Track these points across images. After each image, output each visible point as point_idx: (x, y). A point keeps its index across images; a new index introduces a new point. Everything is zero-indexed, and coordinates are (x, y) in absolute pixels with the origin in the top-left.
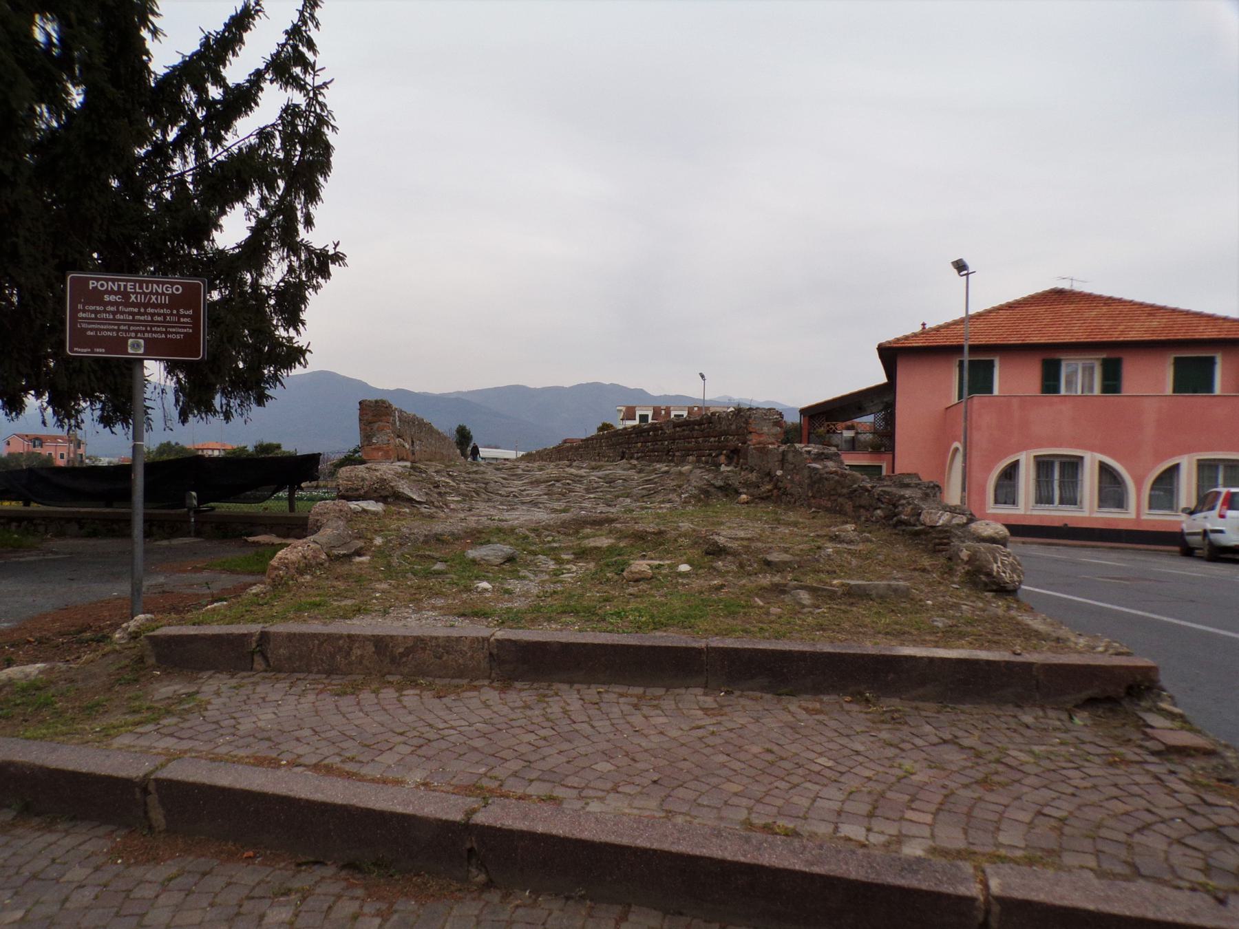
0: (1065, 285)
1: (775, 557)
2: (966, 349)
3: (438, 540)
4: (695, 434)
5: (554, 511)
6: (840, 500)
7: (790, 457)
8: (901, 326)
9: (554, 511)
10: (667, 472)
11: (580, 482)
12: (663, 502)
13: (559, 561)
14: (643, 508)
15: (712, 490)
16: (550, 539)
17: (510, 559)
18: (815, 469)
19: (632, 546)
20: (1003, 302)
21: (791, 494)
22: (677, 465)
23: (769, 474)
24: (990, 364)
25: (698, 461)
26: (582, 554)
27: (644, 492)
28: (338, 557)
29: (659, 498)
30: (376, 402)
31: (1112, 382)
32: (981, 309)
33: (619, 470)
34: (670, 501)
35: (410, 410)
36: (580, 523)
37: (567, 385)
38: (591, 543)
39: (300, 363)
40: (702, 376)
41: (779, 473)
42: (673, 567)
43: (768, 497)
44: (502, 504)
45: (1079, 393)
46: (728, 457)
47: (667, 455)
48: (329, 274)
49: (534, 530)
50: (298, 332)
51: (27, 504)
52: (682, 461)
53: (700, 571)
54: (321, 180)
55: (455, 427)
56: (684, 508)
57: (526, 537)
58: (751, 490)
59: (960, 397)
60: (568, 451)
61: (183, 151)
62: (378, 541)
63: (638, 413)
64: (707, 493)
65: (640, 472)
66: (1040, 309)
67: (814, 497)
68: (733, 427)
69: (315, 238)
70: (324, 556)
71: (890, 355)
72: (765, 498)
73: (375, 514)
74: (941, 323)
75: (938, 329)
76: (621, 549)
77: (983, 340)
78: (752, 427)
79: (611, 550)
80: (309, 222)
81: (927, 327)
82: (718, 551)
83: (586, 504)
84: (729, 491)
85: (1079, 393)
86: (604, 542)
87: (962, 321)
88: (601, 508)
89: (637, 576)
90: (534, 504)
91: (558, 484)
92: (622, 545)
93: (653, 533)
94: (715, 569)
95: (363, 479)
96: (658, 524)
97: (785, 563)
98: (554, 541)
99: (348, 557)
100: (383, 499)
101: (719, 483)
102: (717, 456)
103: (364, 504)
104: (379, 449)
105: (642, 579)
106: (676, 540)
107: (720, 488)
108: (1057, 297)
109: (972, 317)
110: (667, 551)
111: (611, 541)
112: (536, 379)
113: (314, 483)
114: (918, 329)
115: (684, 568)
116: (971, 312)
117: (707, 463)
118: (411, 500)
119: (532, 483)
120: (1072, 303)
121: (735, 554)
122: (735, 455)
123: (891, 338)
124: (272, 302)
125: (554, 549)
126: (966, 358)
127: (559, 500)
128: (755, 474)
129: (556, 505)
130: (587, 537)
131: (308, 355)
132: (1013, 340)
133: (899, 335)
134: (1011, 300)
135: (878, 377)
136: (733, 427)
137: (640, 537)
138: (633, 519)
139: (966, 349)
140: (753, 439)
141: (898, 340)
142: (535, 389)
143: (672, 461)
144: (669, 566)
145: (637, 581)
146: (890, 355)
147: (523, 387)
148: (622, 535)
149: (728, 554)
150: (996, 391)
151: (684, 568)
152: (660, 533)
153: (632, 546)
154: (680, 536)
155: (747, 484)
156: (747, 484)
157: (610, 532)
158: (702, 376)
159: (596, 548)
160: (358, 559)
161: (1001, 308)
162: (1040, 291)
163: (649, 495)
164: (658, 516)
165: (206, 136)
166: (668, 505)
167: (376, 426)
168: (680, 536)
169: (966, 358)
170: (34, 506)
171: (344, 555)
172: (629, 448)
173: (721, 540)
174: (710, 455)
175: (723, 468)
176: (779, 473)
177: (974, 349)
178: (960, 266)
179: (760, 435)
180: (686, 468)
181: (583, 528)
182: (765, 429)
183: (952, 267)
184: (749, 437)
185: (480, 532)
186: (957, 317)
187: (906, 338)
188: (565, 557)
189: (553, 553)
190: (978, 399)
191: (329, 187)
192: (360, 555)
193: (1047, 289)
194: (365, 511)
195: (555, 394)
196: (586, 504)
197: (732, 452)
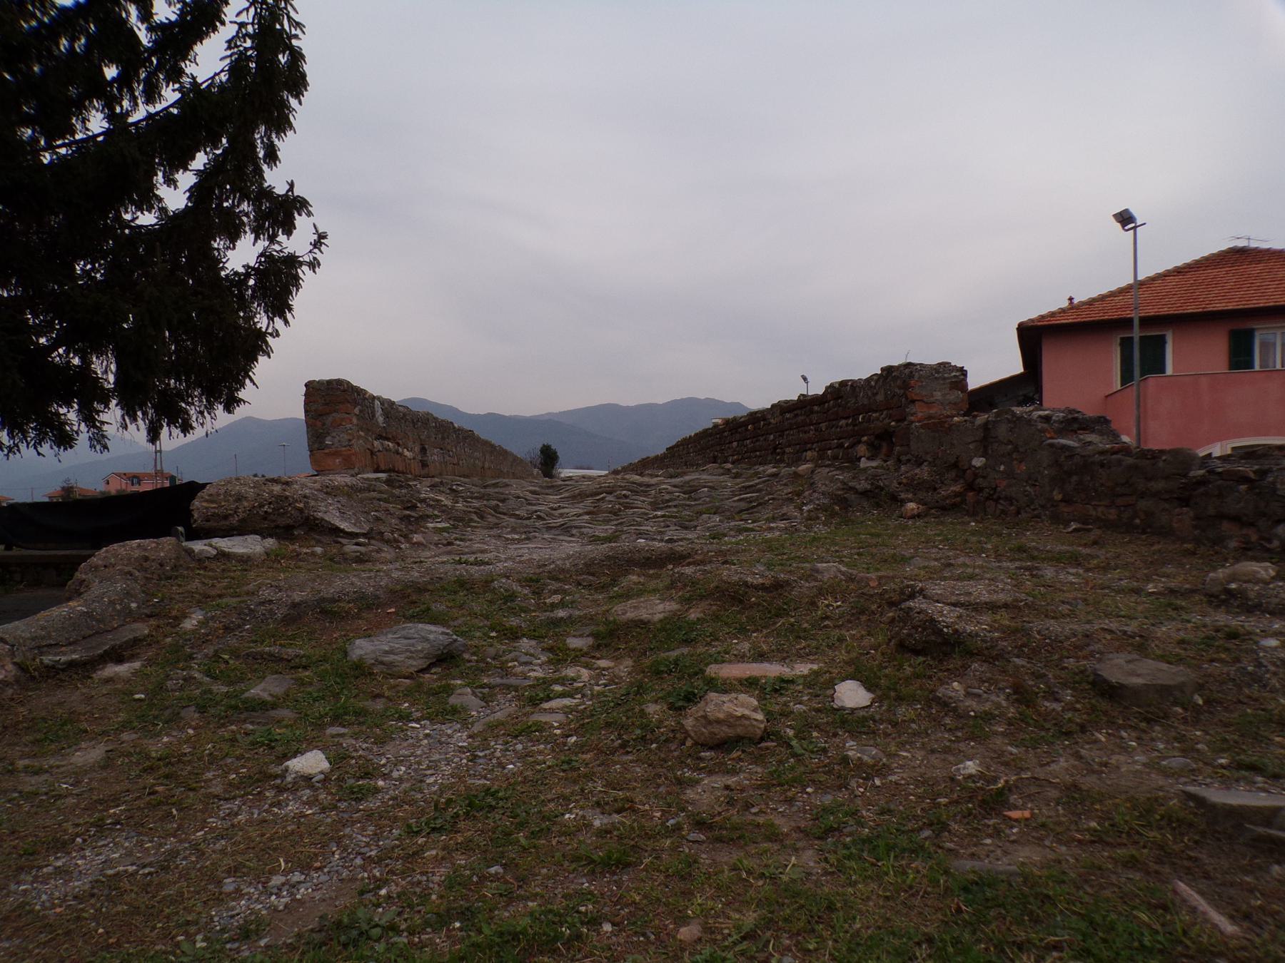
0: (1241, 244)
1: (1120, 668)
2: (1136, 323)
3: (324, 612)
4: (815, 417)
5: (595, 540)
6: (1143, 504)
7: (1002, 431)
8: (1044, 302)
9: (595, 540)
10: (774, 475)
11: (645, 494)
12: (774, 519)
13: (560, 656)
14: (740, 531)
15: (851, 496)
16: (556, 598)
17: (445, 659)
18: (1064, 447)
19: (716, 618)
20: (1170, 267)
21: (1010, 500)
22: (789, 465)
23: (955, 465)
24: (1161, 341)
25: (821, 457)
26: (610, 637)
27: (743, 505)
28: (52, 672)
29: (767, 513)
30: (329, 382)
31: (1240, 356)
32: (1151, 273)
33: (705, 476)
34: (784, 517)
35: (441, 416)
36: (622, 564)
37: (661, 401)
38: (628, 611)
39: (264, 352)
40: (805, 379)
41: (978, 462)
42: (822, 685)
43: (954, 506)
44: (514, 530)
45: (1279, 366)
46: (870, 445)
47: (775, 453)
50: (286, 322)
51: (8, 548)
52: (798, 460)
53: (903, 712)
54: (293, 102)
55: (539, 446)
56: (809, 528)
57: (511, 597)
58: (921, 495)
59: (1127, 377)
60: (644, 465)
61: (131, 91)
64: (844, 503)
65: (737, 476)
66: (1213, 272)
67: (1067, 501)
68: (880, 398)
69: (275, 179)
71: (1033, 337)
72: (945, 509)
74: (1094, 295)
75: (1091, 302)
76: (692, 626)
77: (1151, 311)
79: (672, 630)
80: (272, 156)
81: (1076, 301)
82: (941, 647)
83: (648, 527)
84: (881, 498)
85: (1279, 366)
86: (656, 609)
88: (672, 532)
89: (724, 732)
90: (566, 529)
91: (610, 498)
92: (693, 615)
93: (763, 587)
94: (944, 704)
96: (769, 566)
97: (1164, 691)
98: (562, 605)
99: (85, 668)
100: (284, 532)
101: (863, 485)
102: (852, 446)
103: (224, 544)
104: (336, 454)
105: (736, 742)
106: (813, 604)
107: (865, 494)
108: (1239, 257)
110: (797, 633)
111: (674, 606)
112: (628, 399)
114: (1065, 304)
115: (852, 695)
116: (1140, 278)
117: (835, 458)
118: (336, 531)
119: (574, 497)
120: (1259, 262)
121: (990, 655)
122: (883, 441)
123: (1034, 315)
124: (251, 282)
125: (557, 622)
126: (1136, 333)
127: (607, 521)
128: (925, 467)
129: (601, 530)
130: (627, 596)
132: (1191, 309)
133: (1044, 312)
134: (1179, 264)
135: (1013, 365)
136: (880, 398)
137: (734, 596)
138: (720, 553)
139: (1136, 323)
141: (1042, 317)
143: (781, 461)
144: (811, 681)
145: (722, 745)
146: (1033, 337)
148: (693, 593)
149: (971, 654)
150: (1169, 370)
151: (852, 695)
152: (778, 586)
153: (716, 618)
154: (821, 592)
155: (915, 486)
156: (915, 486)
157: (672, 586)
158: (805, 379)
159: (641, 624)
160: (112, 670)
161: (1167, 274)
162: (1215, 251)
163: (751, 509)
164: (769, 546)
165: (160, 67)
166: (782, 524)
167: (329, 420)
168: (821, 592)
169: (1136, 333)
170: (16, 552)
171: (72, 664)
173: (947, 616)
174: (840, 446)
175: (864, 463)
176: (978, 462)
177: (1146, 322)
178: (1125, 219)
180: (803, 468)
181: (627, 573)
182: (938, 395)
185: (421, 590)
186: (1123, 284)
187: (1052, 314)
188: (574, 643)
189: (550, 633)
190: (1153, 381)
191: (303, 111)
192: (120, 660)
193: (1224, 248)
194: (223, 555)
195: (650, 409)
196: (648, 527)
197: (878, 437)
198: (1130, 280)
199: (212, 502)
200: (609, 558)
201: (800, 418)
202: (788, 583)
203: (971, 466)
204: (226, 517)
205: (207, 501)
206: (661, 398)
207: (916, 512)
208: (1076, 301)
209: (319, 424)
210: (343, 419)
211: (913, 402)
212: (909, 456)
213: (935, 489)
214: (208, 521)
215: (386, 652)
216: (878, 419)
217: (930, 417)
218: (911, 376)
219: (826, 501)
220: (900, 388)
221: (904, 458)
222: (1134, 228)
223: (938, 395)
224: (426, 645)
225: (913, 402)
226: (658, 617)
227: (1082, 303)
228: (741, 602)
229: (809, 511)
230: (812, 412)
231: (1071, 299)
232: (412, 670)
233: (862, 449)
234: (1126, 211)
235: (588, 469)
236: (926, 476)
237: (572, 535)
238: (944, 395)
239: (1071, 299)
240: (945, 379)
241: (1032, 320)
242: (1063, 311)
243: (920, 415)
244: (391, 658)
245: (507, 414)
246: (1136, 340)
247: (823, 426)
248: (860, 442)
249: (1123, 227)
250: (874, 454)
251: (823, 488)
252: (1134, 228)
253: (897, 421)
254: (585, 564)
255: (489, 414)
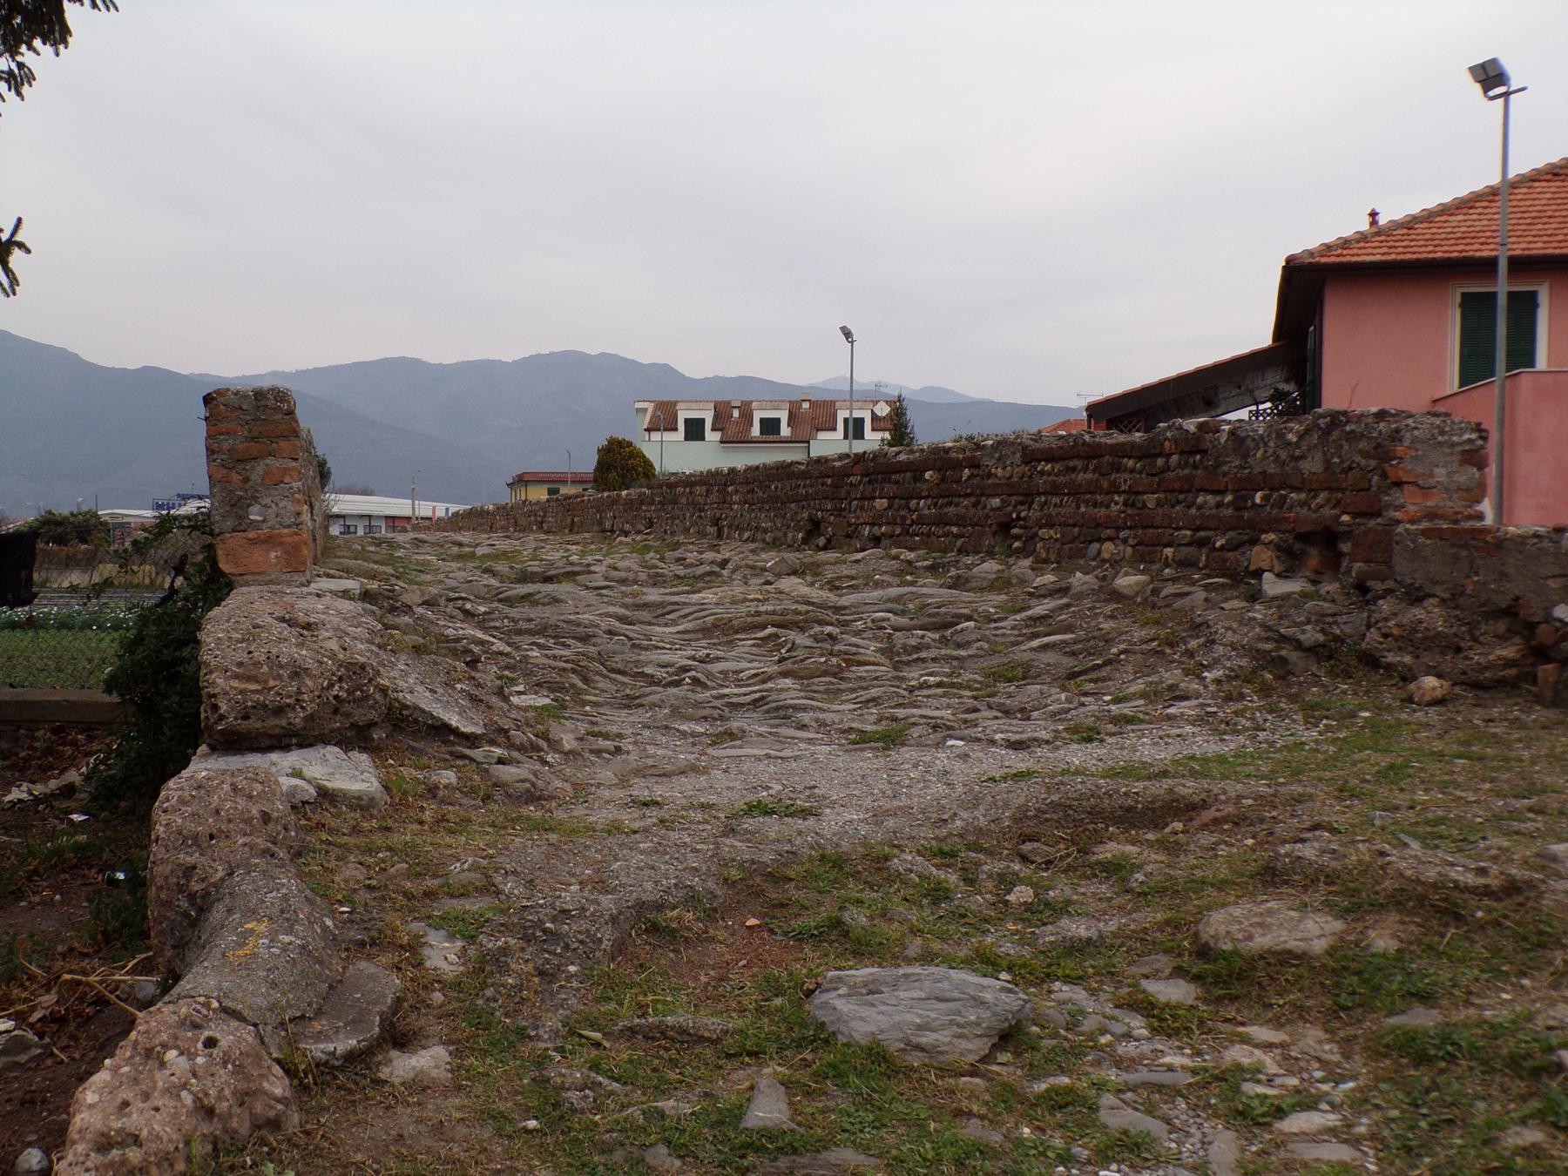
3: (654, 929)
8: (1326, 224)
20: (1540, 164)
23: (1509, 612)
24: (1532, 298)
28: (326, 1069)
30: (259, 394)
40: (847, 334)
48: (65, 32)
49: (943, 855)
62: (443, 955)
63: (842, 415)
70: (278, 1086)
72: (1482, 686)
73: (362, 804)
75: (1410, 223)
77: (1538, 248)
78: (1408, 468)
81: (1383, 220)
87: (1492, 193)
95: (298, 673)
100: (355, 738)
104: (269, 541)
107: (1313, 651)
109: (1514, 185)
112: (442, 348)
113: (21, 612)
116: (1511, 175)
118: (442, 731)
123: (1313, 244)
126: (1502, 287)
131: (16, 259)
133: (1330, 238)
140: (1408, 506)
141: (1328, 247)
142: (125, 373)
147: (417, 360)
150: (1542, 362)
158: (847, 334)
159: (1286, 958)
160: (402, 1066)
167: (258, 471)
169: (1502, 287)
171: (351, 1057)
172: (839, 512)
175: (1272, 586)
177: (1522, 266)
178: (1490, 77)
179: (1426, 490)
183: (1469, 78)
184: (1396, 496)
190: (1525, 380)
195: (482, 375)
198: (1495, 179)
199: (249, 679)
200: (1054, 806)
201: (1081, 477)
202: (1530, 885)
203: (1549, 619)
204: (279, 711)
205: (237, 677)
206: (509, 343)
207: (1439, 694)
208: (1383, 220)
209: (235, 477)
210: (285, 471)
211: (1399, 484)
212: (1390, 584)
213: (1459, 650)
214: (246, 717)
215: (920, 1027)
216: (1303, 504)
217: (1431, 515)
218: (1396, 436)
219: (1244, 662)
220: (1366, 455)
221: (1378, 586)
222: (1506, 95)
223: (1441, 474)
224: (986, 1014)
225: (1399, 484)
226: (1319, 946)
227: (1396, 225)
228: (1458, 917)
229: (1218, 681)
230: (1118, 468)
231: (1373, 214)
232: (972, 1058)
233: (1261, 556)
234: (1494, 62)
235: (365, 492)
236: (1440, 626)
237: (803, 727)
238: (1450, 474)
239: (1373, 214)
240: (1453, 445)
241: (1311, 253)
242: (1362, 238)
243: (1412, 509)
244: (927, 1039)
245: (132, 366)
246: (1502, 301)
247: (1151, 500)
248: (1254, 541)
249: (1486, 91)
250: (1291, 562)
251: (1230, 637)
252: (1506, 95)
253: (1355, 515)
254: (1013, 819)
255: (146, 370)
